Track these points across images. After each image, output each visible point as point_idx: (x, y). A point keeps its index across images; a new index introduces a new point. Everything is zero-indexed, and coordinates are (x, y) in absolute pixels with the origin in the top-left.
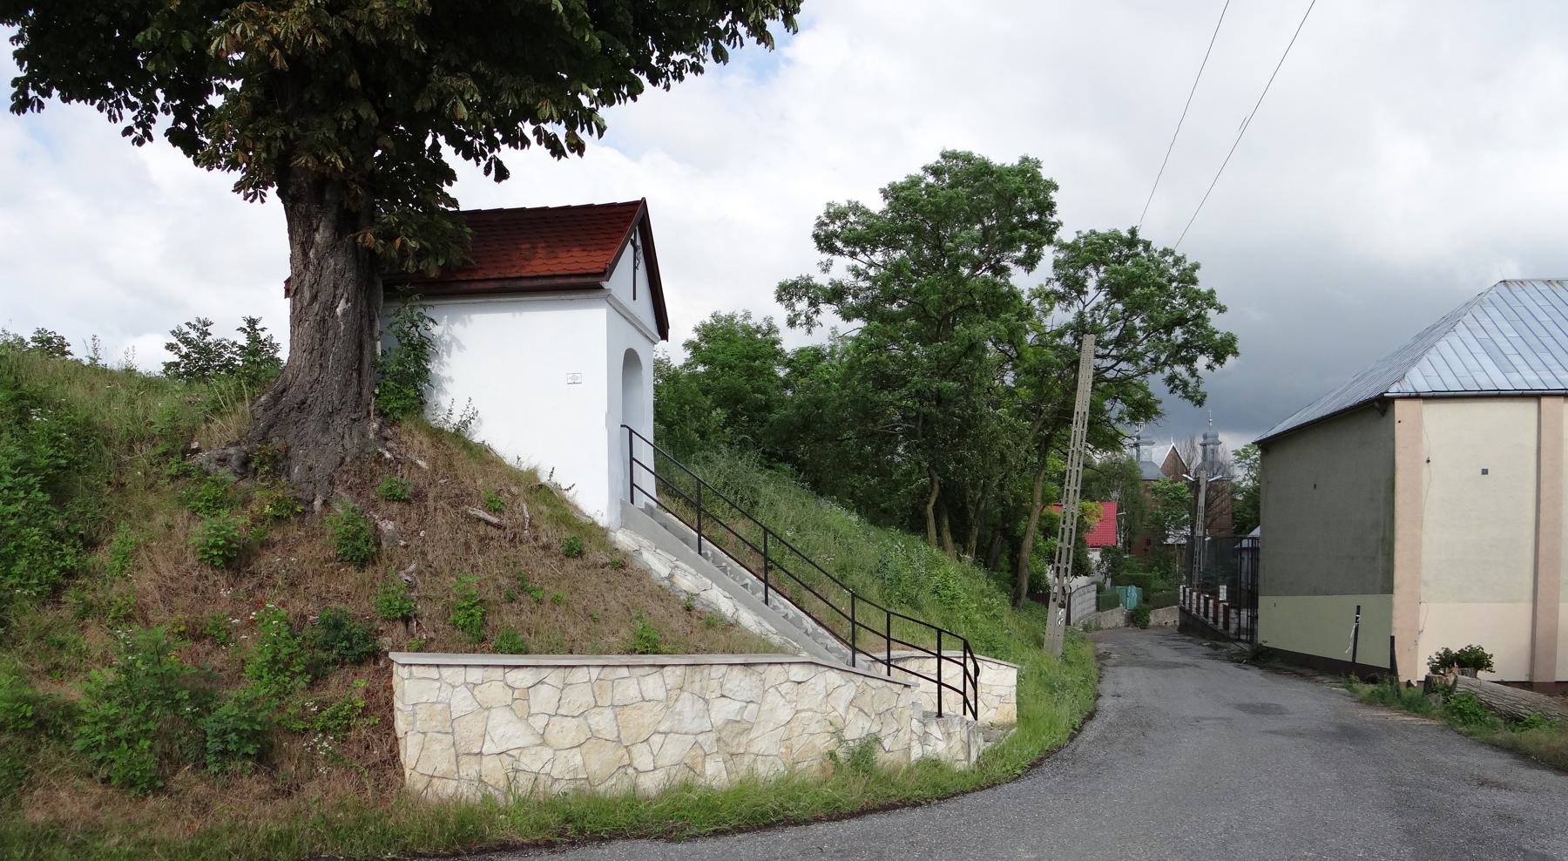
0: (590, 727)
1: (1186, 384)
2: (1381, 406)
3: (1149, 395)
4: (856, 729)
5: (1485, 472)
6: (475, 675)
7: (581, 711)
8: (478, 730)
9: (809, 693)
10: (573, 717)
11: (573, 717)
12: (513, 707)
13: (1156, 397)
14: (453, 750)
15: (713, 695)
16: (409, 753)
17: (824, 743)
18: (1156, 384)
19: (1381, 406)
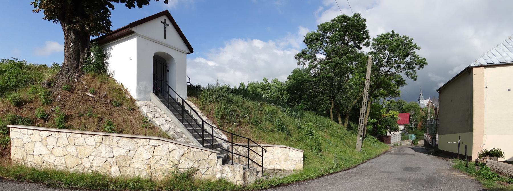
0: (67, 151)
1: (411, 74)
2: (469, 71)
3: (402, 79)
4: (185, 166)
5: (509, 90)
6: (30, 132)
7: (64, 145)
8: (32, 147)
9: (160, 150)
10: (61, 147)
11: (61, 147)
12: (42, 142)
13: (404, 79)
14: (25, 152)
15: (114, 146)
16: (13, 152)
17: (168, 167)
18: (403, 75)
19: (469, 71)
